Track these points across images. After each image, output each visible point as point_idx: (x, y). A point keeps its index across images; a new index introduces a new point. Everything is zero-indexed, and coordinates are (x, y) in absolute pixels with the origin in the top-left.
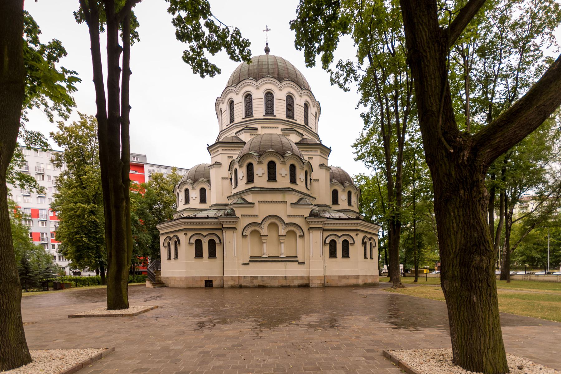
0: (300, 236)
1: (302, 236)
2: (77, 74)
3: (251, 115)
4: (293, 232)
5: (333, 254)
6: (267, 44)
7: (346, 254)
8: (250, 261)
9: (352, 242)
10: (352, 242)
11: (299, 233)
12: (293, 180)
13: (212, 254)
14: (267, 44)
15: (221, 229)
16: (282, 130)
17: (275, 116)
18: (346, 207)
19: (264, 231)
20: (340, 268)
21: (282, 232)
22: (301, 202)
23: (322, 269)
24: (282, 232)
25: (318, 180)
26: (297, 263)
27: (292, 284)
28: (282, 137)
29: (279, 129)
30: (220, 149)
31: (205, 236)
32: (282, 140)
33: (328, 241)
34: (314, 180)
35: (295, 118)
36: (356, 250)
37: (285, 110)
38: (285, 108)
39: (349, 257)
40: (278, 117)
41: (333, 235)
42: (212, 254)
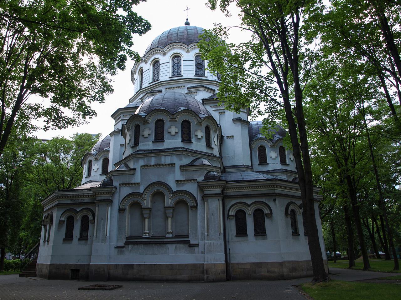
0: (192, 207)
1: (195, 208)
2: (213, 110)
3: (158, 79)
4: (184, 203)
5: (241, 231)
6: (187, 19)
7: (260, 231)
8: (127, 244)
9: (269, 212)
10: (269, 212)
11: (191, 203)
12: (187, 138)
13: (84, 237)
14: (187, 19)
15: (93, 203)
16: (188, 88)
17: (182, 76)
18: (279, 166)
19: (146, 203)
20: (250, 251)
21: (169, 202)
22: (194, 164)
23: (222, 255)
24: (169, 202)
25: (231, 137)
26: (187, 245)
27: (179, 277)
28: (186, 95)
29: (186, 87)
30: (121, 116)
31: (249, 206)
32: (188, 99)
33: (232, 213)
34: (228, 137)
35: (206, 76)
36: (277, 225)
37: (194, 69)
38: (194, 67)
39: (265, 235)
40: (185, 76)
41: (236, 204)
42: (84, 237)
